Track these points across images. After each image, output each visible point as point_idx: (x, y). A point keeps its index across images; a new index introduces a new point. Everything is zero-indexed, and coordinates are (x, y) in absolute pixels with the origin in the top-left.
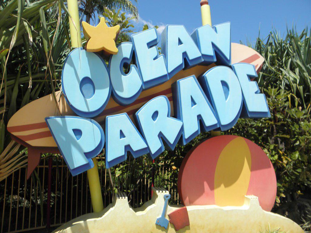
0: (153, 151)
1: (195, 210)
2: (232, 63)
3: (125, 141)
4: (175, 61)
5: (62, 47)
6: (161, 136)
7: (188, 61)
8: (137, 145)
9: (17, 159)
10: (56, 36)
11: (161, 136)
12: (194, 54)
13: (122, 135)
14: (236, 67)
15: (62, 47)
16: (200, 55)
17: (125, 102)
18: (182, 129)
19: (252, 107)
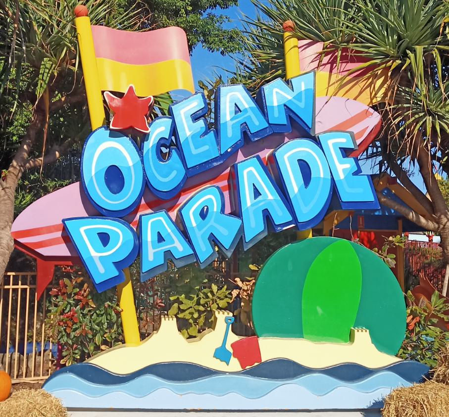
0: (202, 258)
1: (105, 178)
2: (318, 130)
3: (165, 247)
4: (231, 134)
5: (428, 197)
6: (214, 240)
7: (250, 135)
8: (179, 248)
9: (27, 367)
10: (363, 55)
11: (214, 240)
12: (257, 123)
13: (161, 239)
14: (322, 138)
15: (428, 197)
16: (267, 125)
17: (163, 197)
18: (242, 229)
19: (348, 194)
